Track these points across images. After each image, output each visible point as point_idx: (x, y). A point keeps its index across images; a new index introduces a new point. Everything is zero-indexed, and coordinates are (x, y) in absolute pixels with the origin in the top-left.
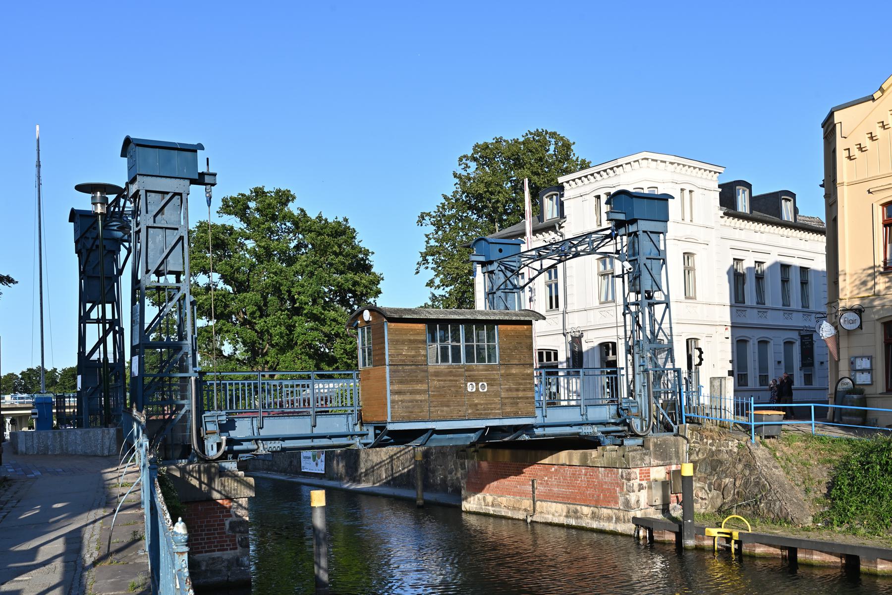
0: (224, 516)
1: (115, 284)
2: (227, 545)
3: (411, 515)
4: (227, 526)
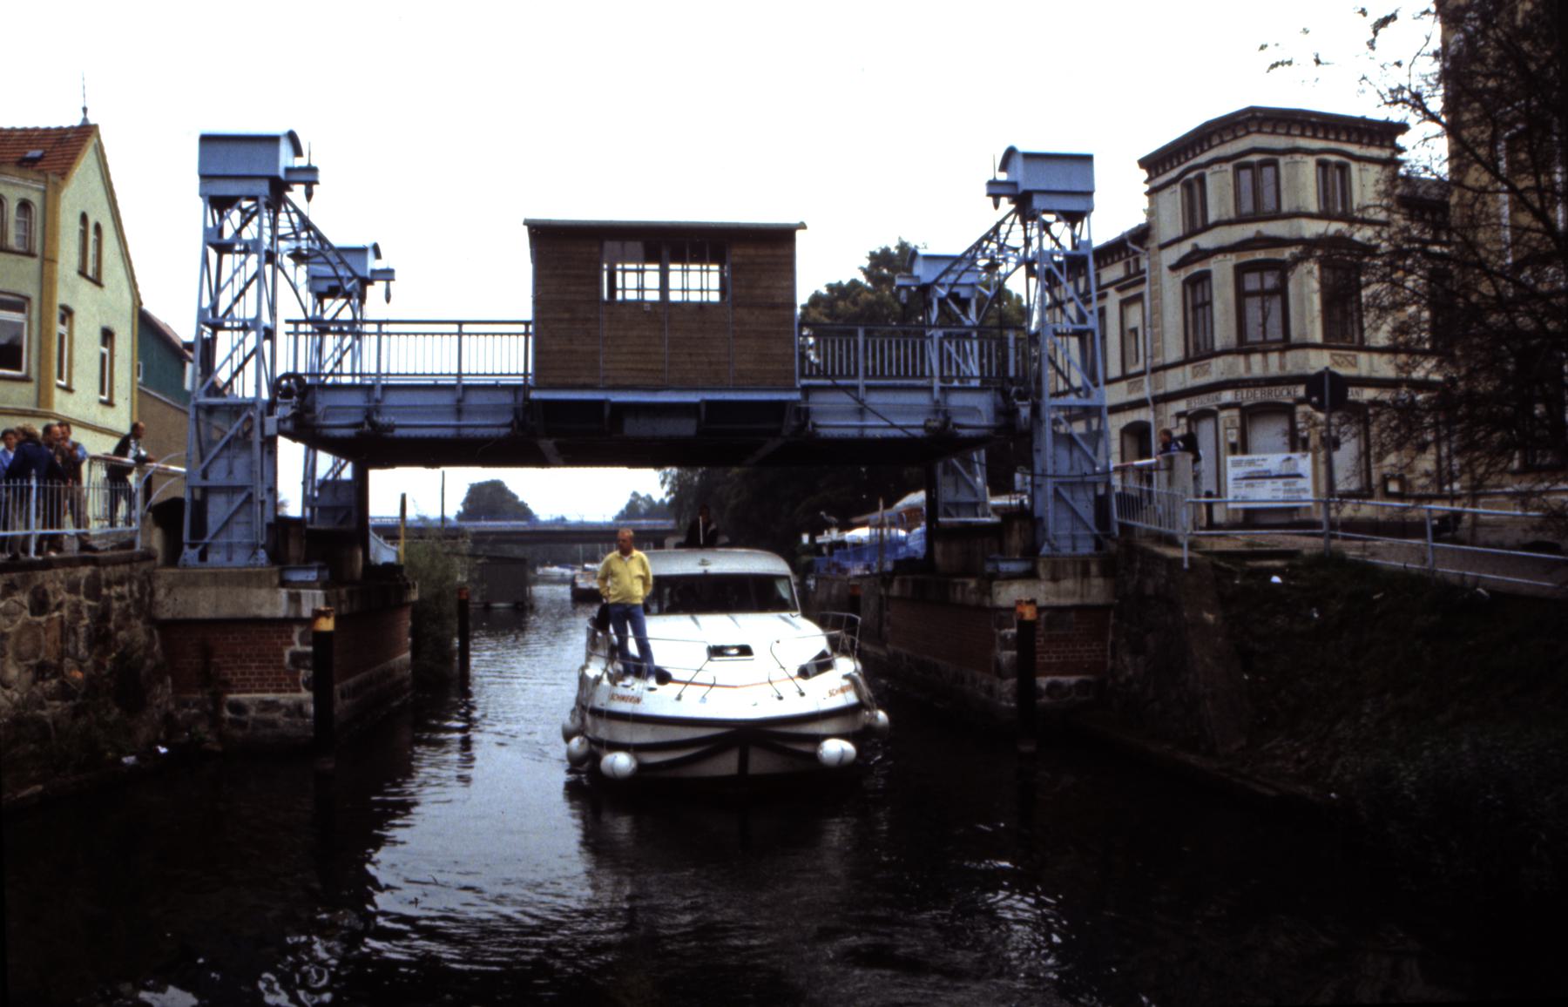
4: (287, 658)
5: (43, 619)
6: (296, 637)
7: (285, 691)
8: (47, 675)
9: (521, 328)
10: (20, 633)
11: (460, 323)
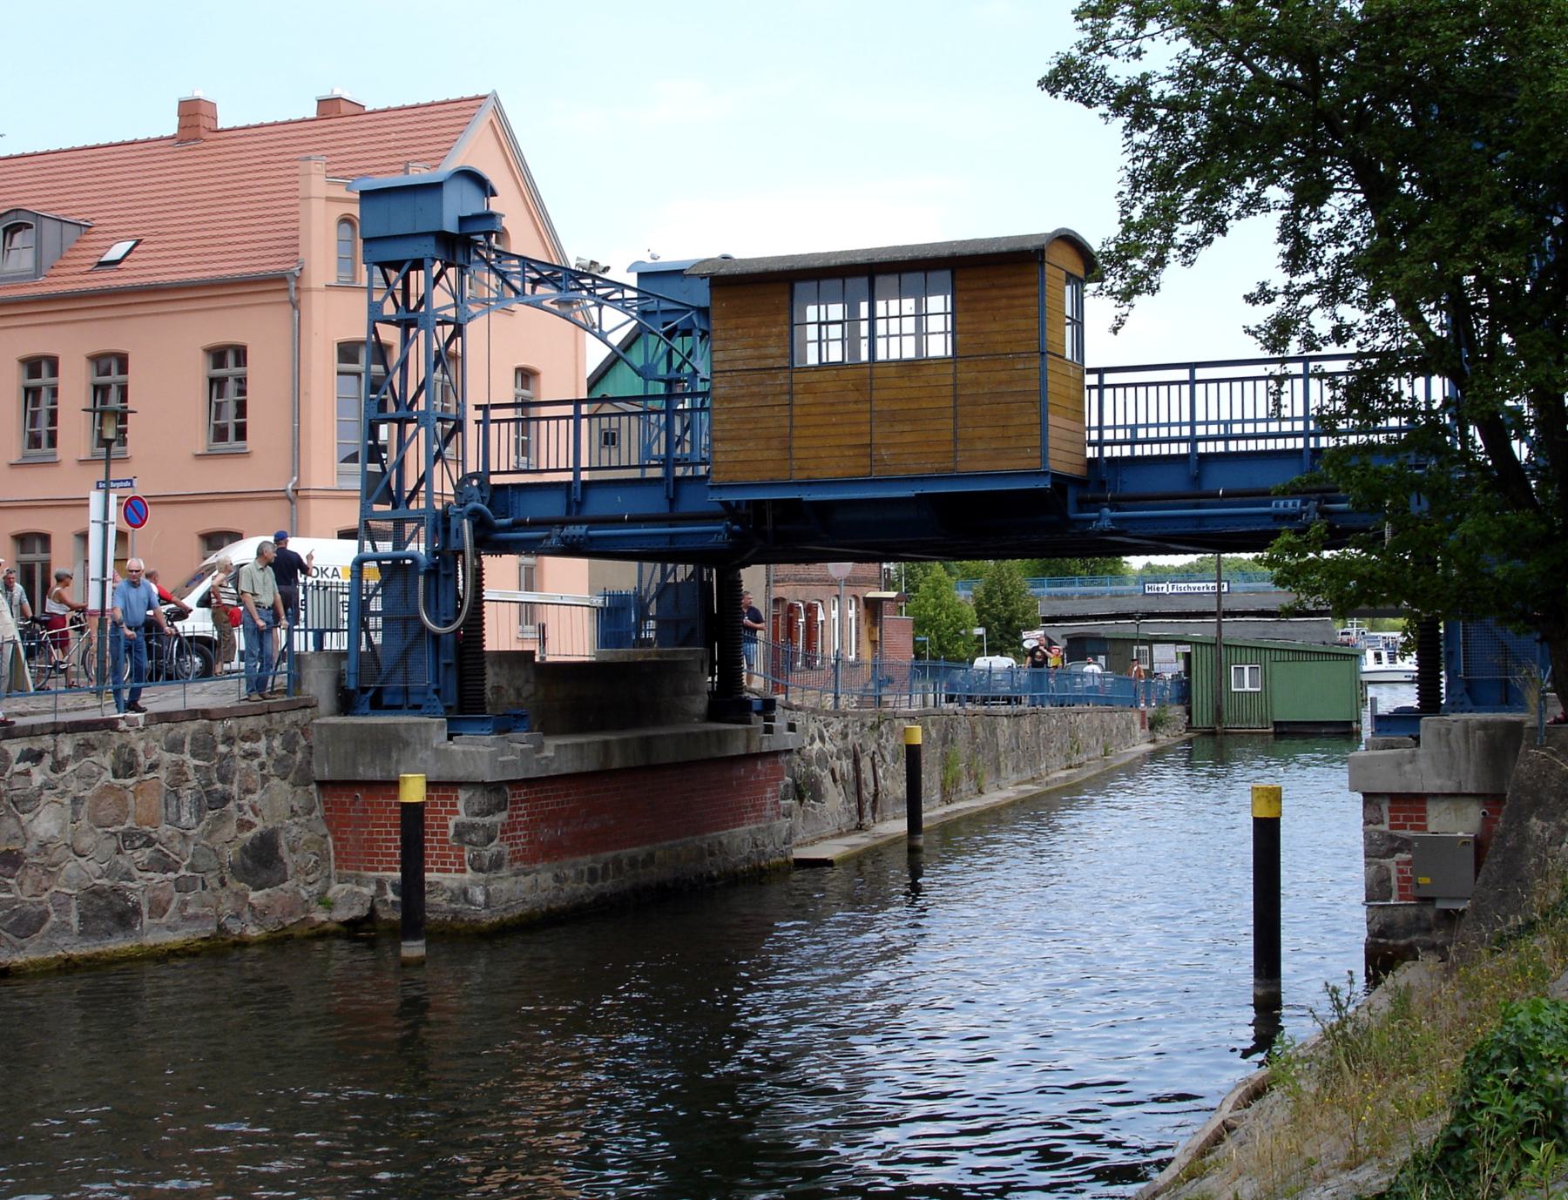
0: (447, 812)
1: (364, 634)
2: (451, 864)
3: (884, 1029)
4: (451, 832)
5: (130, 781)
6: (460, 806)
7: (449, 871)
8: (137, 843)
9: (569, 410)
10: (99, 797)
11: (1192, 366)
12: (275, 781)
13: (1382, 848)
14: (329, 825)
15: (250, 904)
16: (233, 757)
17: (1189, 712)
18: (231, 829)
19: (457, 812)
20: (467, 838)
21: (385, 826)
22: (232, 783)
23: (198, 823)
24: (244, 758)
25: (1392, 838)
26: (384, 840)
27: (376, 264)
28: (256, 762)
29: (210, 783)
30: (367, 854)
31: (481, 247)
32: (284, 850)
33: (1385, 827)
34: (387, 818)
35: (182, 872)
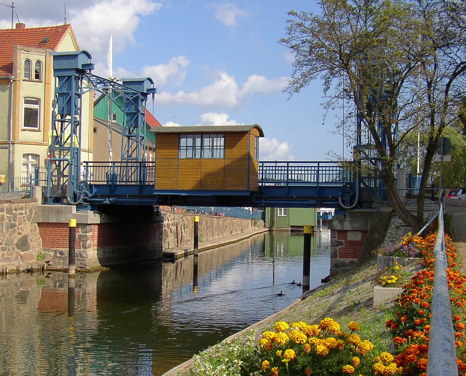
12: (27, 221)
13: (336, 244)
14: (41, 235)
15: (21, 255)
16: (17, 214)
17: (264, 222)
18: (16, 235)
19: (79, 232)
20: (81, 239)
21: (57, 235)
22: (16, 221)
23: (7, 232)
24: (19, 214)
25: (338, 242)
26: (57, 239)
27: (57, 76)
28: (22, 216)
29: (11, 221)
30: (51, 243)
31: (87, 73)
32: (29, 241)
33: (336, 239)
34: (58, 233)
35: (3, 245)
